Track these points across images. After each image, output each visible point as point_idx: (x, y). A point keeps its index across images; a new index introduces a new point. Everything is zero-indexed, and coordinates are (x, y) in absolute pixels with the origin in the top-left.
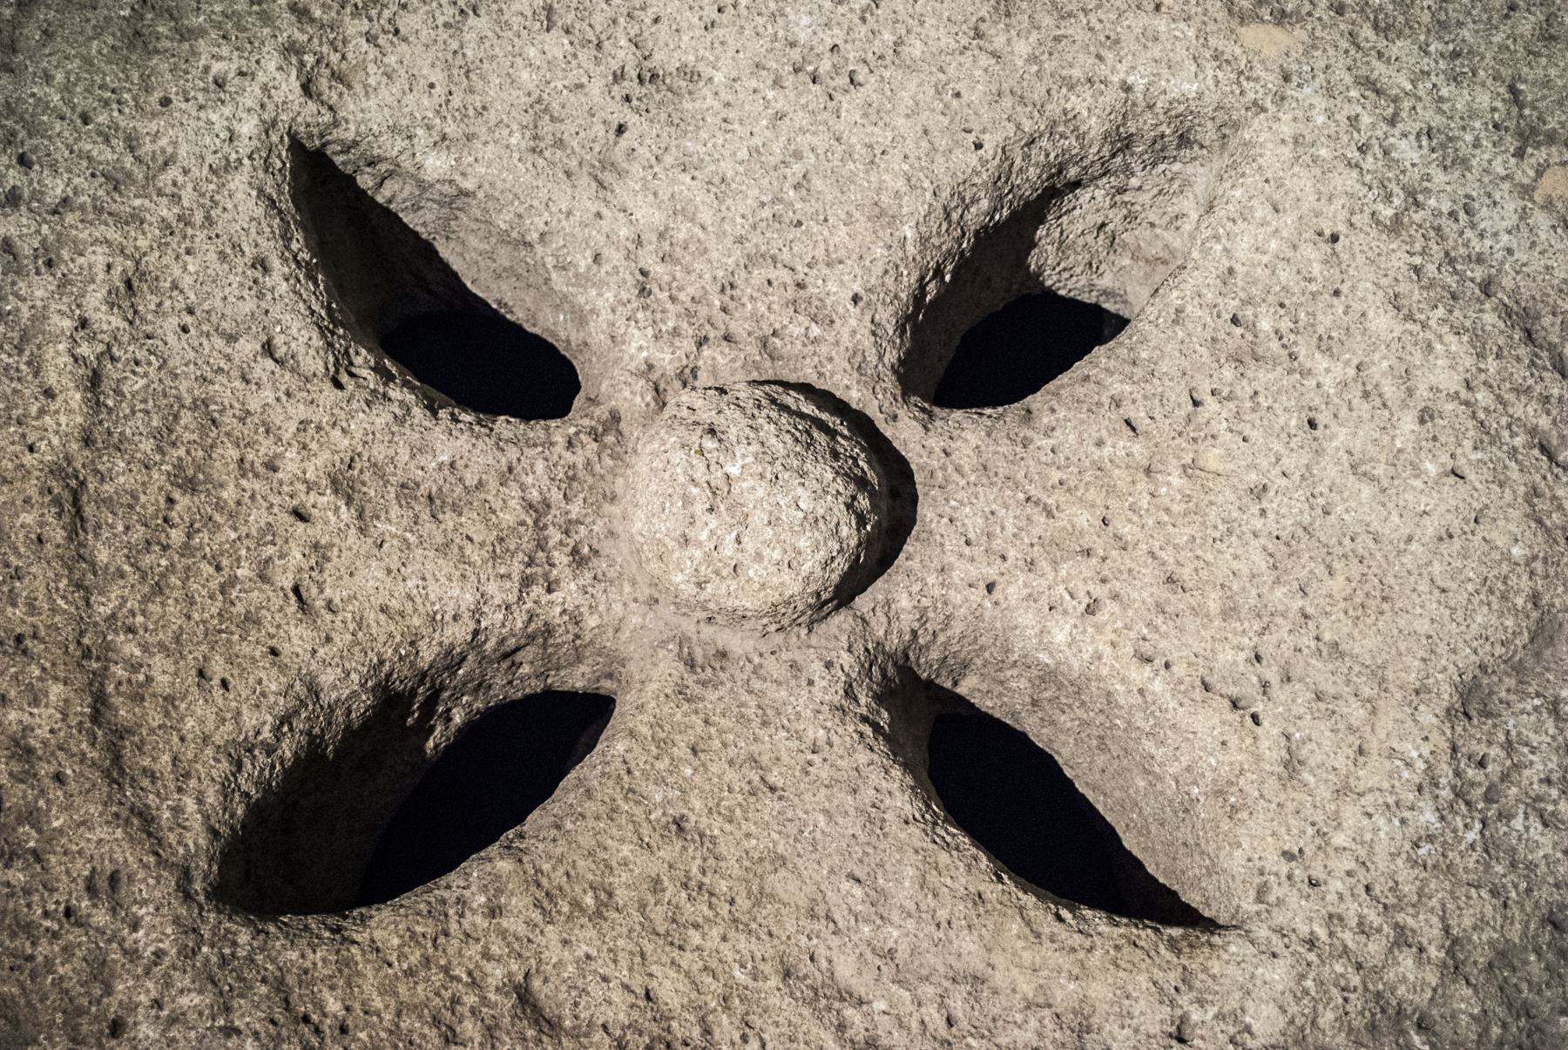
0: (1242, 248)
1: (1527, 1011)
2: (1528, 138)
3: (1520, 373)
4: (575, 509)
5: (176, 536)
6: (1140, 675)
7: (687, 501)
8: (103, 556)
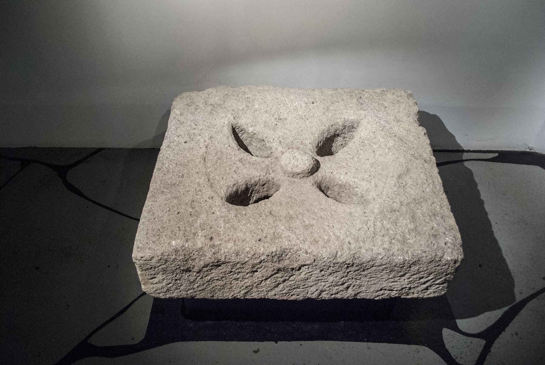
0: (362, 134)
1: (412, 210)
2: (398, 121)
3: (401, 144)
4: (272, 166)
5: (218, 164)
6: (353, 180)
7: (290, 158)
8: (208, 165)
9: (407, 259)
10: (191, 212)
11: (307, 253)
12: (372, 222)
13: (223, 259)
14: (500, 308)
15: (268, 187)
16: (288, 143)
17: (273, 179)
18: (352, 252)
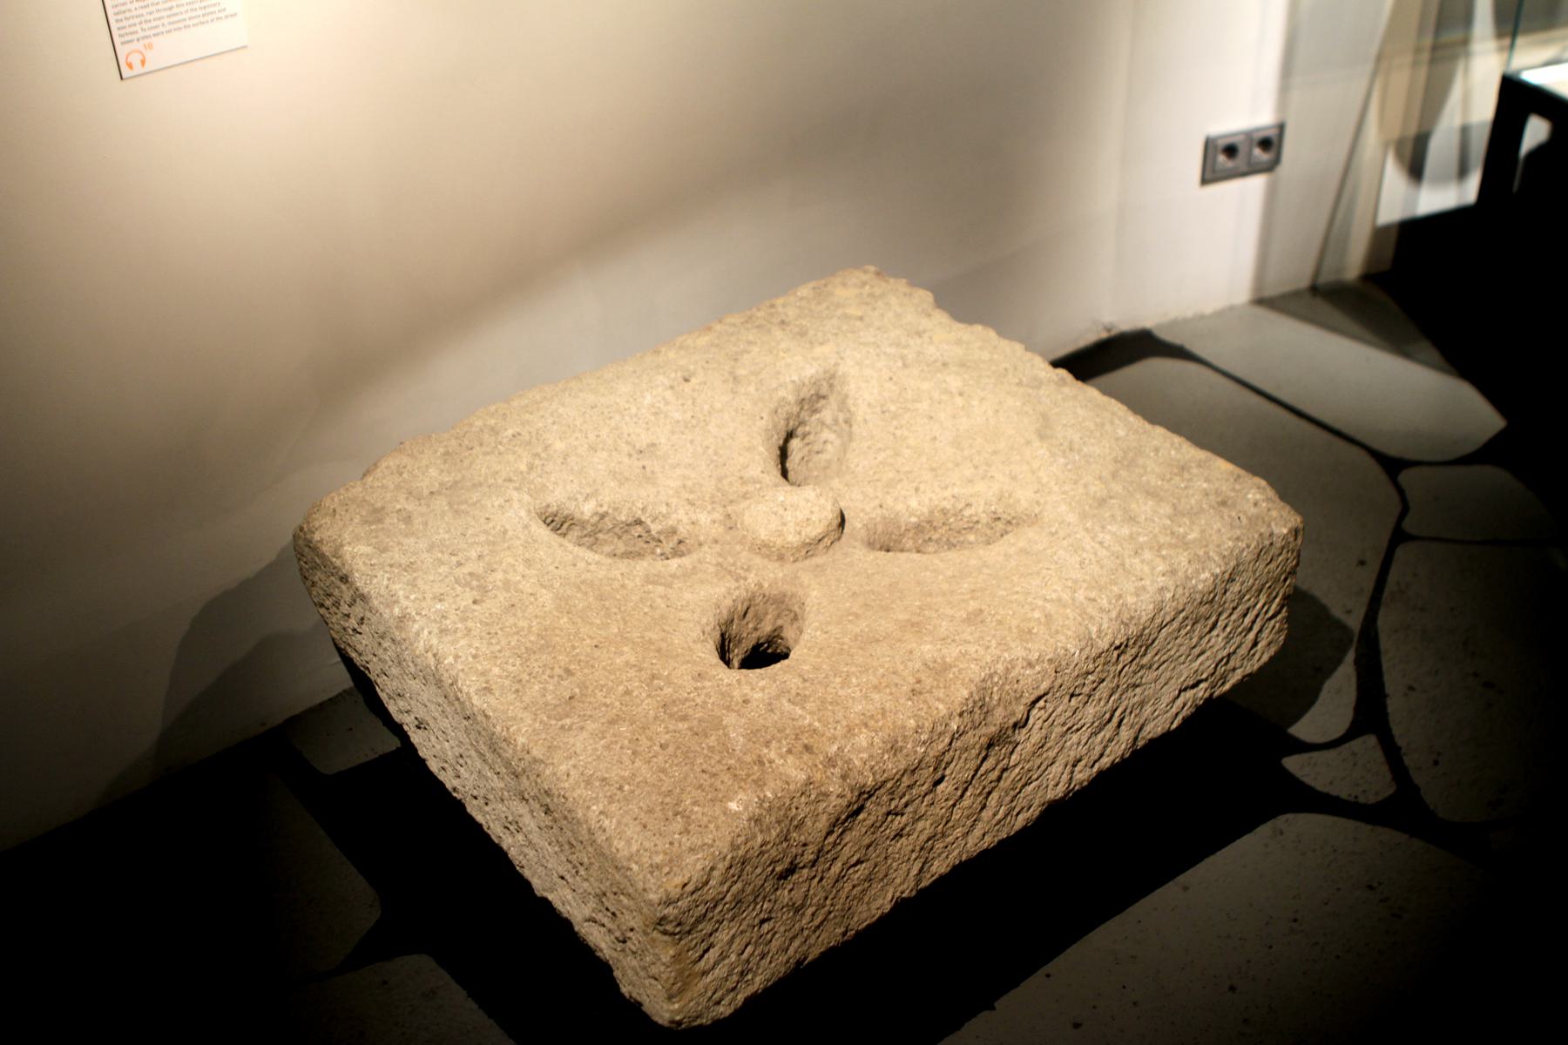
6: (948, 493)
9: (1218, 571)
10: (690, 729)
11: (1030, 665)
12: (1088, 539)
13: (870, 782)
14: (1339, 661)
15: (756, 616)
16: (713, 496)
17: (760, 586)
18: (1114, 614)
